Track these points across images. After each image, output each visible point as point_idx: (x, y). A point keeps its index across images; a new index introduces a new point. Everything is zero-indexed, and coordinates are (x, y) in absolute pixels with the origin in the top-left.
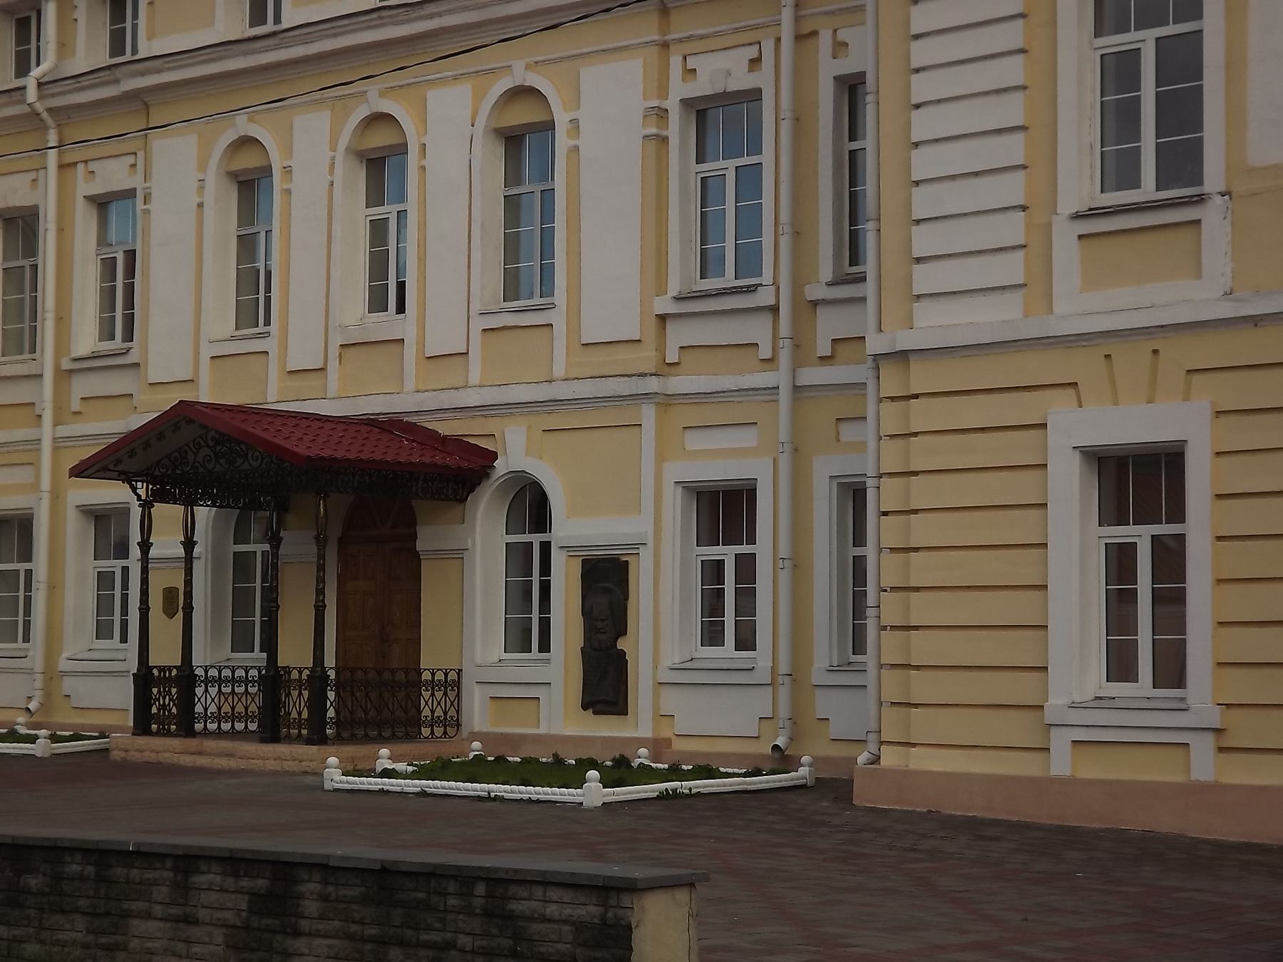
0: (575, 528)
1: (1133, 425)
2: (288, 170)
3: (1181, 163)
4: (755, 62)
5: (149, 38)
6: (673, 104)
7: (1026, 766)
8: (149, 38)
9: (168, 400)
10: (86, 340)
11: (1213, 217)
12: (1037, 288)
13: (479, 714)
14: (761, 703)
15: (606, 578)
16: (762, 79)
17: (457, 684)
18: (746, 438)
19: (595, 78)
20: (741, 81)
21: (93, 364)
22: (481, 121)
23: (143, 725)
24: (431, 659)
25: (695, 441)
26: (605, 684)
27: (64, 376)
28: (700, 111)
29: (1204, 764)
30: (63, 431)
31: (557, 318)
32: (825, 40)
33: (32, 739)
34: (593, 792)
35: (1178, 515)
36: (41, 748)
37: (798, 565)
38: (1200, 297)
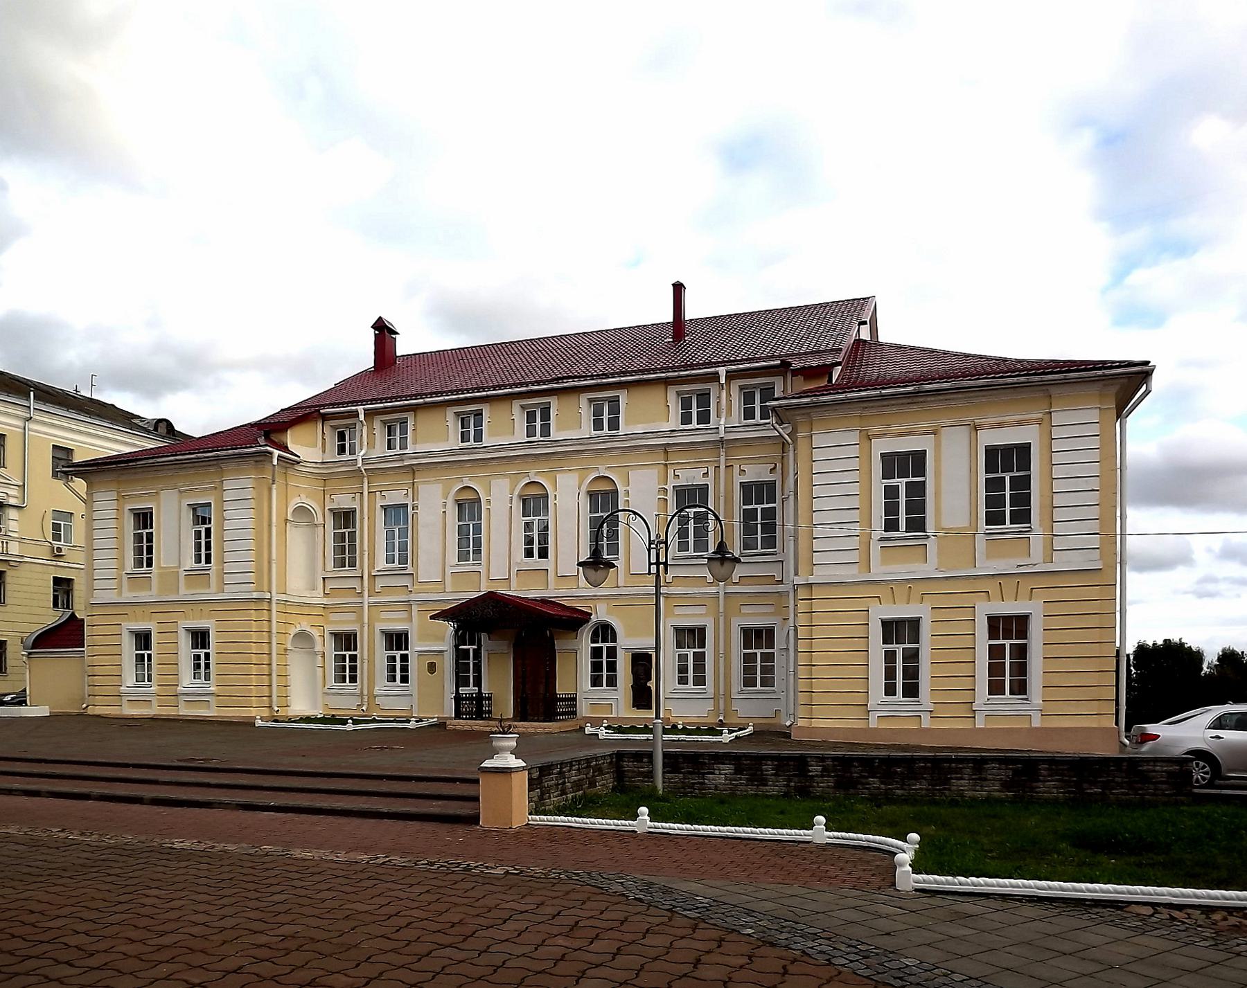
0: (629, 641)
1: (141, 626)
2: (489, 502)
3: (917, 524)
5: (415, 442)
6: (669, 487)
7: (967, 724)
8: (415, 442)
9: (485, 588)
10: (381, 564)
11: (931, 544)
12: (120, 594)
13: (584, 709)
14: (710, 705)
15: (642, 663)
16: (709, 481)
17: (575, 699)
18: (702, 610)
19: (634, 475)
20: (701, 481)
21: (384, 574)
22: (584, 488)
23: (458, 714)
24: (561, 690)
25: (678, 611)
26: (642, 697)
27: (373, 577)
28: (681, 492)
29: (926, 723)
30: (372, 599)
32: (736, 467)
33: (408, 721)
34: (350, 727)
35: (916, 640)
36: (412, 725)
37: (371, 662)
38: (928, 569)
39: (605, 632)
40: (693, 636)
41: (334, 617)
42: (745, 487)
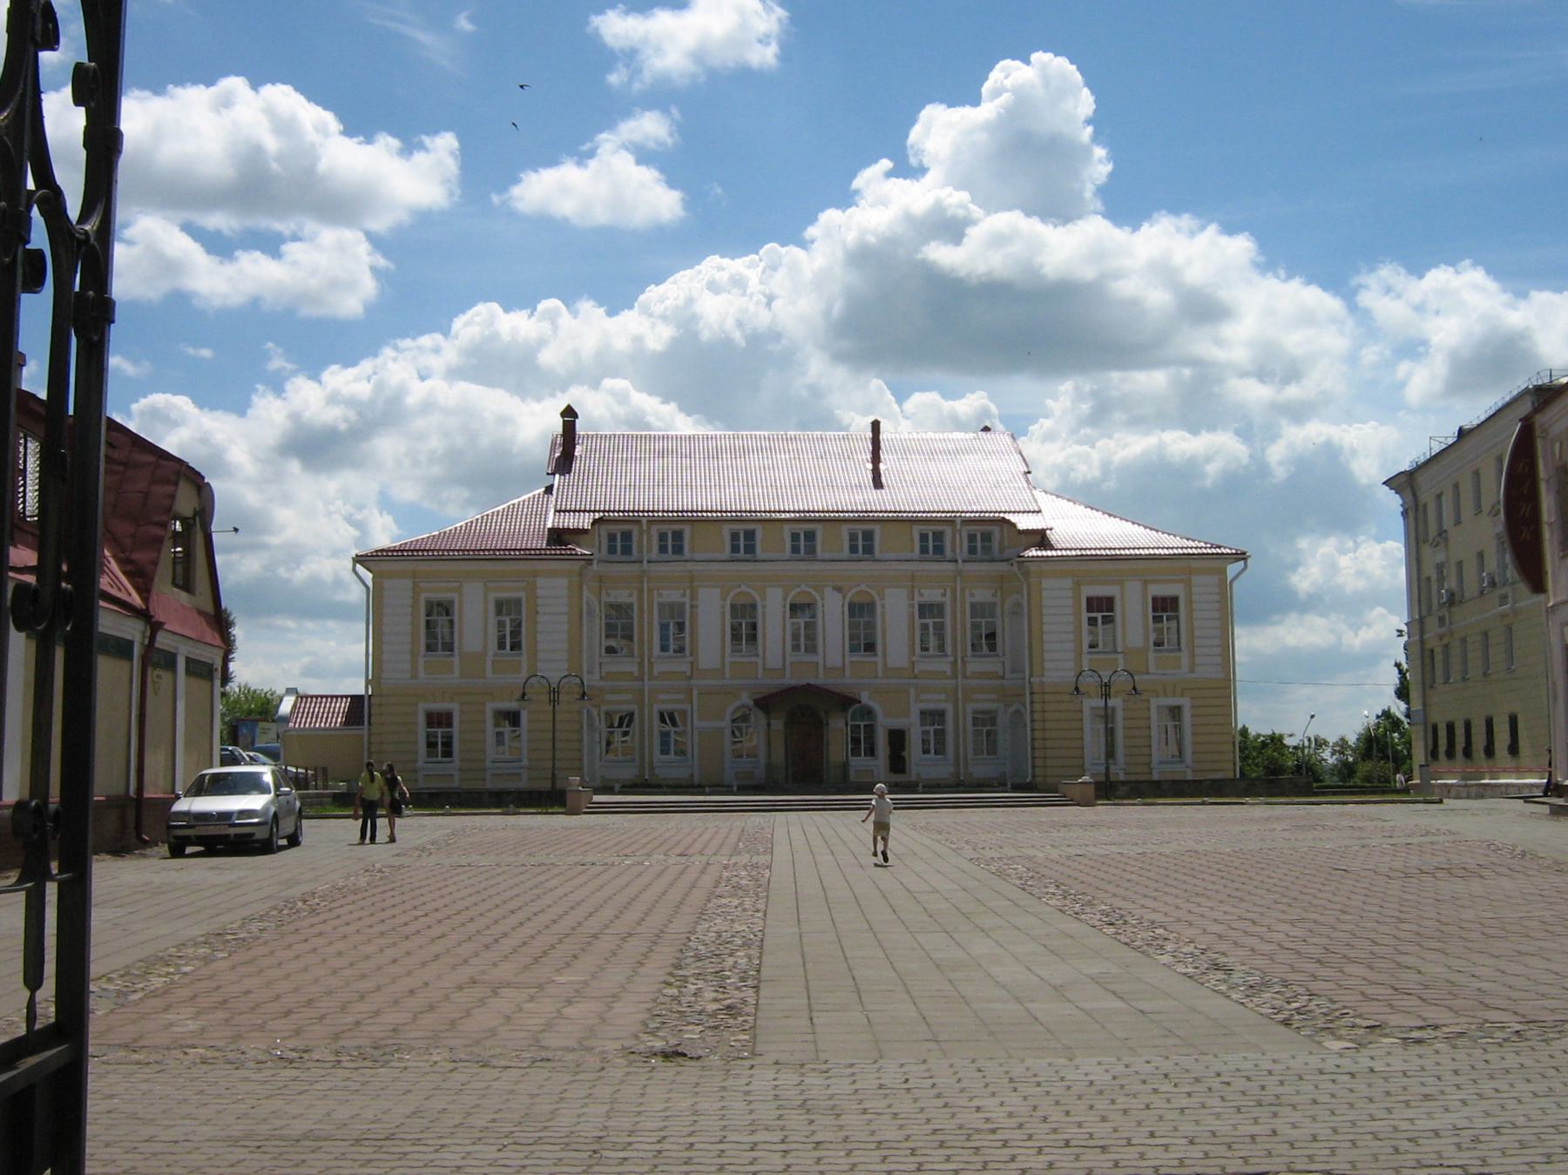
0: (884, 722)
4: (944, 595)
15: (897, 739)
25: (924, 697)
31: (524, 659)
39: (869, 713)
40: (933, 717)
41: (608, 697)
42: (973, 606)
